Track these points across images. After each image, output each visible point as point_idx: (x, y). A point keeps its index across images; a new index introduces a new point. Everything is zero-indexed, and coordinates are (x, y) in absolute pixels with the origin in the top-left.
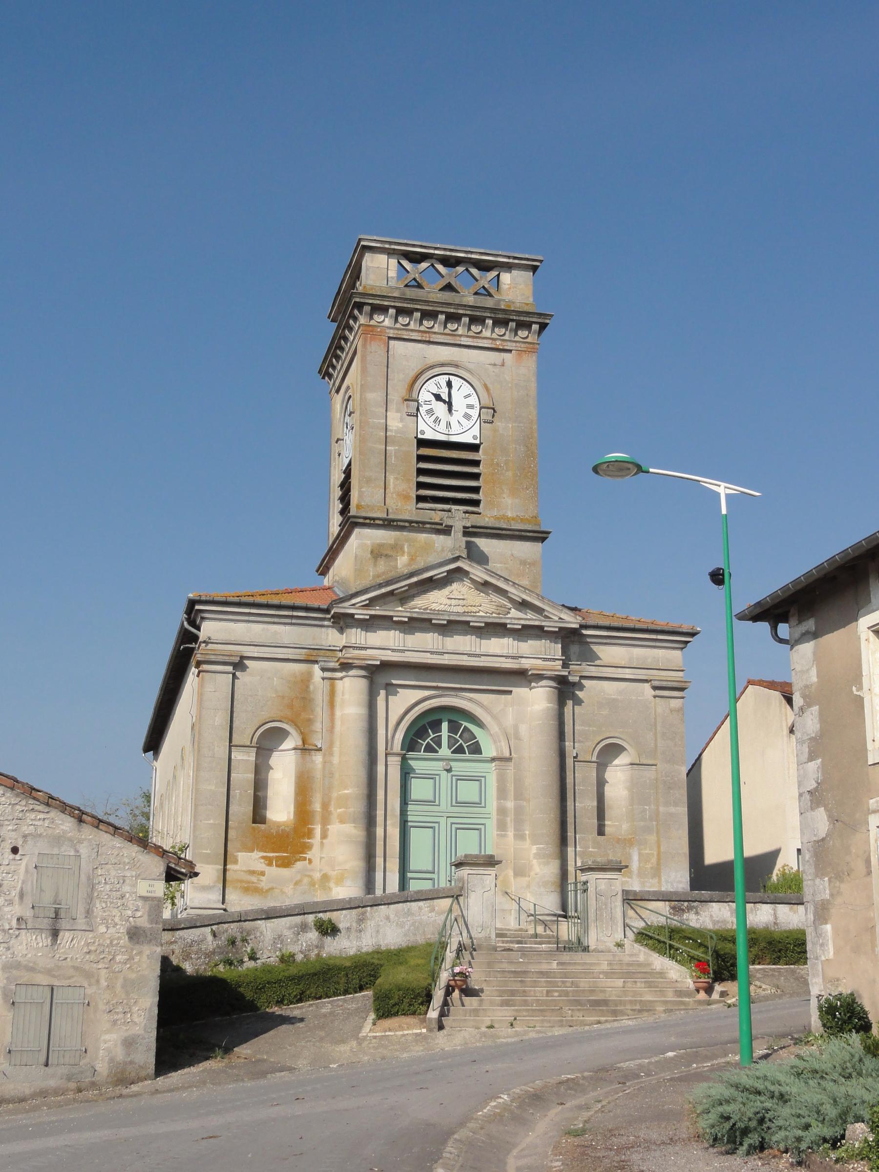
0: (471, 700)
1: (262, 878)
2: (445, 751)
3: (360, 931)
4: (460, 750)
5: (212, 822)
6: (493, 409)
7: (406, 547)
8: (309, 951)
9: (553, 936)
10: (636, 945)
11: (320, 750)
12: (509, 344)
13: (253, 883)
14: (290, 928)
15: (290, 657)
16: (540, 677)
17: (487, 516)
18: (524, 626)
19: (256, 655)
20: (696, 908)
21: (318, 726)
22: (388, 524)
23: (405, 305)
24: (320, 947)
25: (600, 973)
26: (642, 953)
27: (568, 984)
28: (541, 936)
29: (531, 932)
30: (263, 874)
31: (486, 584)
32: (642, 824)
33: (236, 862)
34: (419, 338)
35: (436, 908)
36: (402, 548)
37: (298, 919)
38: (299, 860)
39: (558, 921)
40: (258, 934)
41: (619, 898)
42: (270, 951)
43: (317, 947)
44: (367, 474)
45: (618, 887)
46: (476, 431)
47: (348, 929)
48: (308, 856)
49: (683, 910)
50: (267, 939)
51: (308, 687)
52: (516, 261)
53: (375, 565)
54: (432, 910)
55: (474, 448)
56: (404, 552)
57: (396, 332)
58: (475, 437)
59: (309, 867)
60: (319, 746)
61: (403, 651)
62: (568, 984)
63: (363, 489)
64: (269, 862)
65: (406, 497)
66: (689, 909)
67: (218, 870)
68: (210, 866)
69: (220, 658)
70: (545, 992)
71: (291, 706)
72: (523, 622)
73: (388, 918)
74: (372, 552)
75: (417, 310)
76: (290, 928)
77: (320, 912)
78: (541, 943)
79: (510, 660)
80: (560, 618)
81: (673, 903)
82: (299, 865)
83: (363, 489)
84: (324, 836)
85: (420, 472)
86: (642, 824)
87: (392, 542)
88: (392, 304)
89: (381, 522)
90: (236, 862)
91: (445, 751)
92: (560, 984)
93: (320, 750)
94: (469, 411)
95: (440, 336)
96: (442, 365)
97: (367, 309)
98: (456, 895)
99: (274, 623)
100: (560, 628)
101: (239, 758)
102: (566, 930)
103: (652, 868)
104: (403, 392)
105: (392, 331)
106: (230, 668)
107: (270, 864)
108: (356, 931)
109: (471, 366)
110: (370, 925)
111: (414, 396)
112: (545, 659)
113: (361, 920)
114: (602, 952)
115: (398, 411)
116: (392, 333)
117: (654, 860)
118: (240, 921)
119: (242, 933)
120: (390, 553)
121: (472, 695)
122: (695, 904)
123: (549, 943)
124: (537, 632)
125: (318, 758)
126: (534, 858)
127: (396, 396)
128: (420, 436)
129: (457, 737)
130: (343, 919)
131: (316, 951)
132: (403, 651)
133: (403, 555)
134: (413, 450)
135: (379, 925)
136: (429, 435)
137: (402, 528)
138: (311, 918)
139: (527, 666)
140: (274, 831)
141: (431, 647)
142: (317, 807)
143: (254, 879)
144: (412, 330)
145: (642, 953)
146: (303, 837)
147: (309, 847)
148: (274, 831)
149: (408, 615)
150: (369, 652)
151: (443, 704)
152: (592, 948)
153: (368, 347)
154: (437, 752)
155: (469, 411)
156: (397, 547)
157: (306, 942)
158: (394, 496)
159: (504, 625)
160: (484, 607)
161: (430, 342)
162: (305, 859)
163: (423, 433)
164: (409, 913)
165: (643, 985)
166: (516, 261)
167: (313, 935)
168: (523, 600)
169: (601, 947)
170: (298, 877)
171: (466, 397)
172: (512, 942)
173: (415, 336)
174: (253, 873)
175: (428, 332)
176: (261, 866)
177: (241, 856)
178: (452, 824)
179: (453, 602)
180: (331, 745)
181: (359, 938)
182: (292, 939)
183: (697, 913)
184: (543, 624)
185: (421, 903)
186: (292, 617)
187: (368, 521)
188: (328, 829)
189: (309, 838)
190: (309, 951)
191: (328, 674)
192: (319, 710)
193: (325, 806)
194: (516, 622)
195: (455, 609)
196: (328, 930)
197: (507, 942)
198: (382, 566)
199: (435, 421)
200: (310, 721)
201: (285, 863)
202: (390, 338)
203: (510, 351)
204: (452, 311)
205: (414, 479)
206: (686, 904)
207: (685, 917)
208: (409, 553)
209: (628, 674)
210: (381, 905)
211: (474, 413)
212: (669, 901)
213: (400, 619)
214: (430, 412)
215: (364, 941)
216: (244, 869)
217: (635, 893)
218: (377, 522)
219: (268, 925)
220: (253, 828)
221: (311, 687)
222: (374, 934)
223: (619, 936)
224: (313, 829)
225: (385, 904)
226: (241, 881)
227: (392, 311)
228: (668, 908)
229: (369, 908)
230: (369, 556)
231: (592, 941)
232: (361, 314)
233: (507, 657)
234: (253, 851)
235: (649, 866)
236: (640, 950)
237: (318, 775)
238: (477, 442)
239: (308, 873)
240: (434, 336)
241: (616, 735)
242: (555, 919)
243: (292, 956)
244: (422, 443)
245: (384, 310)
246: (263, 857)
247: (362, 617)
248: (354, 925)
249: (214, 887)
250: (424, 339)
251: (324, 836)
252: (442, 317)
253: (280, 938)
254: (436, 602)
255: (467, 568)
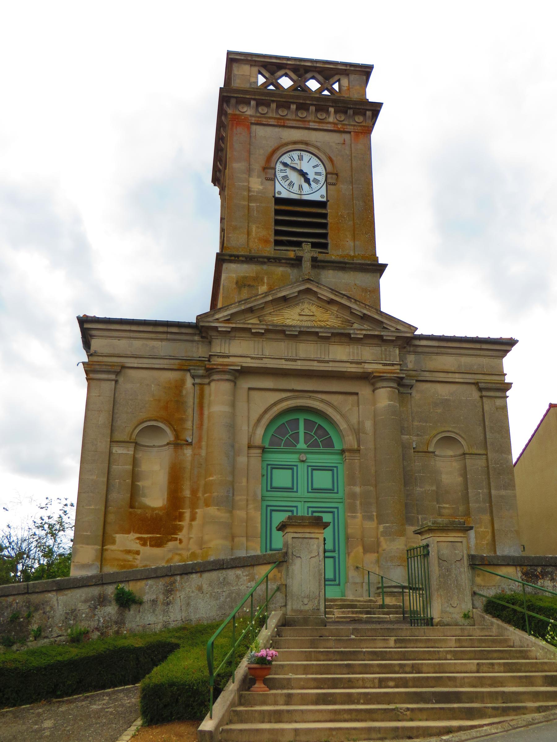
0: (322, 401)
1: (139, 557)
2: (301, 445)
3: (168, 604)
4: (315, 445)
5: (93, 507)
6: (337, 174)
7: (265, 279)
8: (107, 627)
9: (400, 606)
10: (488, 617)
11: (190, 444)
12: (348, 127)
13: (129, 561)
14: (85, 601)
15: (166, 367)
16: (381, 379)
17: (333, 254)
18: (365, 336)
19: (136, 365)
20: (551, 573)
21: (189, 424)
22: (250, 259)
23: (263, 98)
24: (120, 622)
25: (447, 652)
26: (495, 626)
27: (408, 669)
28: (388, 606)
29: (380, 602)
30: (138, 553)
31: (331, 302)
32: (477, 505)
33: (114, 542)
34: (276, 123)
35: (257, 577)
36: (262, 280)
37: (95, 591)
38: (171, 540)
39: (403, 592)
40: (48, 609)
41: (466, 562)
42: (60, 628)
43: (116, 623)
44: (233, 223)
45: (462, 552)
46: (323, 191)
47: (154, 602)
48: (179, 537)
49: (537, 577)
50: (58, 615)
51: (181, 392)
52: (352, 68)
53: (240, 293)
54: (252, 579)
55: (322, 204)
56: (264, 283)
57: (257, 119)
58: (322, 196)
59: (180, 546)
60: (190, 440)
61: (261, 359)
62: (408, 669)
63: (230, 235)
64: (144, 542)
65: (266, 241)
66: (544, 575)
67: (96, 550)
68: (90, 547)
69: (104, 368)
70: (376, 681)
71: (166, 408)
72: (364, 332)
73: (200, 589)
74: (237, 283)
75: (273, 101)
76: (85, 601)
77: (121, 582)
78: (388, 613)
79: (354, 365)
80: (397, 329)
81: (525, 569)
82: (171, 545)
83: (230, 235)
84: (193, 518)
85: (277, 222)
86: (477, 505)
87: (254, 275)
88: (253, 97)
89: (244, 259)
90: (114, 542)
91: (301, 445)
92: (397, 669)
93: (190, 444)
94: (317, 177)
95: (292, 122)
96: (295, 143)
97: (233, 101)
98: (281, 560)
99: (152, 339)
100: (398, 337)
101: (120, 452)
102: (413, 601)
103: (487, 544)
104: (262, 163)
105: (253, 119)
106: (113, 377)
107: (144, 544)
108: (163, 604)
109: (318, 144)
110: (180, 597)
111: (272, 165)
112: (385, 365)
113: (169, 591)
114: (448, 625)
115: (259, 177)
116: (253, 120)
117: (489, 537)
118: (28, 593)
119: (28, 607)
120: (252, 283)
121: (324, 397)
122: (550, 569)
123: (396, 613)
124: (376, 341)
125: (188, 452)
126: (382, 536)
127: (257, 167)
128: (277, 195)
129: (312, 434)
130: (148, 590)
131: (115, 628)
132: (261, 359)
133: (263, 285)
134: (272, 206)
135: (189, 597)
136: (285, 194)
137: (263, 263)
138: (110, 590)
139: (370, 370)
140: (149, 515)
141: (286, 354)
142: (187, 493)
143: (129, 557)
144: (270, 118)
145: (495, 626)
146: (175, 519)
147: (180, 529)
148: (149, 515)
149: (265, 327)
150: (231, 360)
151: (299, 404)
152: (436, 620)
153: (235, 130)
154: (296, 446)
155: (317, 177)
156: (258, 279)
157: (104, 617)
158: (256, 240)
159: (348, 335)
160: (328, 319)
161: (284, 126)
162: (176, 539)
163: (280, 193)
164: (225, 583)
165: (502, 669)
166: (352, 68)
167: (111, 610)
168: (364, 314)
169: (446, 620)
170: (170, 555)
171: (314, 167)
172: (361, 613)
173: (272, 122)
174: (129, 552)
175: (283, 119)
176: (136, 546)
177: (119, 537)
178: (309, 507)
179: (305, 318)
180: (200, 439)
181: (166, 612)
182: (87, 614)
183: (552, 579)
184: (382, 334)
185: (239, 572)
186: (167, 333)
187: (233, 258)
188: (196, 513)
189: (180, 521)
190: (107, 627)
191: (198, 381)
192: (190, 411)
193: (194, 492)
194: (358, 332)
195: (306, 324)
196: (126, 601)
197: (357, 612)
198: (245, 294)
199: (289, 185)
200: (182, 421)
201: (158, 543)
202: (252, 124)
203: (350, 132)
204: (301, 101)
205: (272, 227)
206: (539, 569)
207: (539, 584)
208: (268, 284)
209: (457, 378)
210: (192, 573)
211: (322, 179)
212: (520, 565)
213: (257, 331)
214: (285, 178)
215: (172, 615)
216: (121, 549)
217: (482, 558)
218: (241, 258)
219: (61, 598)
220: (131, 513)
221: (184, 392)
222: (184, 608)
223: (467, 606)
224: (183, 513)
225: (196, 572)
226: (118, 560)
227: (253, 103)
228: (520, 574)
229: (178, 578)
230: (235, 286)
231: (436, 611)
232: (229, 108)
233: (351, 363)
234: (129, 533)
235: (485, 542)
236: (492, 624)
237: (188, 465)
238: (325, 199)
239: (179, 552)
240: (288, 122)
241: (450, 429)
242: (401, 590)
243: (86, 633)
244: (279, 201)
245: (247, 102)
246: (138, 538)
247: (224, 329)
248: (161, 597)
249: (92, 565)
250: (279, 124)
251: (193, 518)
252: (293, 107)
253: (73, 613)
254: (292, 317)
255: (315, 289)
